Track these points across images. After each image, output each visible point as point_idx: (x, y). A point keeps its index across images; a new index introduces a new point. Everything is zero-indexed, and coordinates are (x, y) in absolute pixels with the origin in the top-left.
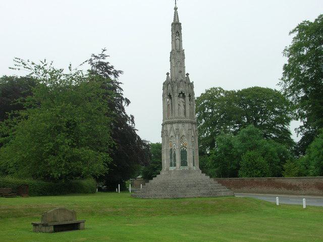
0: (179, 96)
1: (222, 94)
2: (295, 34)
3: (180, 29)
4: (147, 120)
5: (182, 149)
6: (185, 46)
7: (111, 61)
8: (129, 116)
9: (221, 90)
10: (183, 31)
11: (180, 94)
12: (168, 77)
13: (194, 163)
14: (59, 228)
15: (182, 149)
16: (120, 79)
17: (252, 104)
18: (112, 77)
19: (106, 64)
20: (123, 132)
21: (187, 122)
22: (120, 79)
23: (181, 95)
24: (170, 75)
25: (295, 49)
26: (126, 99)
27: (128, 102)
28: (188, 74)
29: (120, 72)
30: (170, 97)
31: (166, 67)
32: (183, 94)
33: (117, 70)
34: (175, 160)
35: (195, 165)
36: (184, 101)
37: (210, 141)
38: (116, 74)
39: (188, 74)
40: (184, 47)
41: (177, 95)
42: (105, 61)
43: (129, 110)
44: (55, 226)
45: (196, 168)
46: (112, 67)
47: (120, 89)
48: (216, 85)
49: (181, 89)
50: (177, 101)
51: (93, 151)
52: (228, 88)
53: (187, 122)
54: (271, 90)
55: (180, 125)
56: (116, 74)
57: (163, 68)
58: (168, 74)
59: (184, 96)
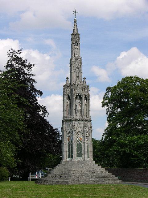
0: (76, 98)
1: (138, 83)
3: (79, 39)
5: (78, 142)
6: (83, 54)
10: (81, 42)
11: (77, 96)
13: (88, 154)
14: (77, 43)
15: (78, 142)
18: (26, 71)
21: (82, 120)
22: (33, 70)
23: (78, 97)
24: (69, 79)
27: (41, 93)
28: (84, 79)
29: (34, 65)
30: (69, 98)
32: (80, 96)
35: (89, 156)
36: (80, 102)
38: (30, 67)
39: (84, 79)
41: (74, 97)
42: (19, 56)
46: (25, 62)
49: (78, 92)
51: (74, 118)
53: (82, 120)
55: (77, 123)
56: (30, 67)
58: (67, 78)
59: (80, 98)
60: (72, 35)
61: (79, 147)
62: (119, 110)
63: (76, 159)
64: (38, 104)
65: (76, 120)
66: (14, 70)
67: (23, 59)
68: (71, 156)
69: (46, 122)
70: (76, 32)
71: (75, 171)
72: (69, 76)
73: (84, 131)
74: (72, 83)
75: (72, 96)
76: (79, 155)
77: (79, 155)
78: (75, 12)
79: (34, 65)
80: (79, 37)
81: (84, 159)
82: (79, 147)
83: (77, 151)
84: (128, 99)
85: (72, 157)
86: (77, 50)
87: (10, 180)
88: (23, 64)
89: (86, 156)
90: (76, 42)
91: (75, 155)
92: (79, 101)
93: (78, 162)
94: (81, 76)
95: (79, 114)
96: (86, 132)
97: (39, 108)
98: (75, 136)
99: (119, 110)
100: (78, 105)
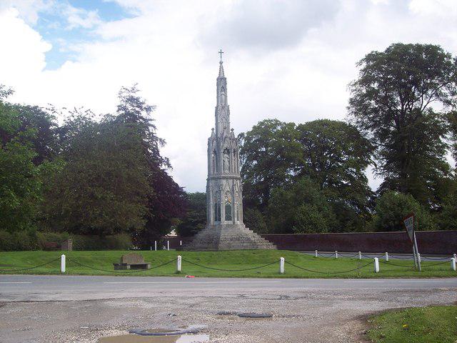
2: (364, 64)
4: (187, 163)
7: (141, 95)
8: (163, 158)
9: (277, 123)
10: (228, 86)
12: (213, 132)
16: (152, 115)
17: (318, 145)
18: (144, 114)
19: (137, 99)
20: (164, 184)
21: (230, 178)
22: (152, 115)
24: (215, 131)
25: (365, 81)
26: (161, 140)
27: (163, 142)
28: (232, 130)
29: (154, 107)
31: (212, 123)
33: (150, 105)
34: (220, 216)
37: (263, 187)
38: (148, 109)
40: (229, 102)
42: (135, 95)
43: (163, 152)
44: (131, 266)
45: (239, 223)
46: (143, 103)
47: (152, 126)
48: (271, 116)
49: (226, 145)
50: (224, 158)
52: (285, 119)
54: (344, 124)
57: (208, 124)
58: (213, 129)
59: (228, 153)
60: (217, 79)
61: (228, 208)
62: (255, 162)
63: (224, 222)
64: (159, 155)
65: (224, 178)
66: (128, 113)
67: (141, 100)
68: (218, 218)
69: (170, 179)
70: (222, 75)
71: (225, 234)
72: (214, 127)
73: (233, 190)
74: (219, 136)
75: (219, 149)
76: (228, 218)
77: (228, 218)
78: (221, 53)
79: (154, 107)
80: (226, 82)
81: (234, 222)
82: (228, 208)
83: (226, 213)
84: (266, 147)
85: (220, 220)
86: (223, 97)
87: (63, 269)
88: (140, 105)
89: (236, 219)
90: (223, 87)
91: (223, 218)
92: (227, 156)
93: (228, 225)
94: (229, 126)
95: (227, 171)
96: (235, 192)
97: (161, 161)
98: (223, 196)
99: (255, 162)
100: (226, 160)
